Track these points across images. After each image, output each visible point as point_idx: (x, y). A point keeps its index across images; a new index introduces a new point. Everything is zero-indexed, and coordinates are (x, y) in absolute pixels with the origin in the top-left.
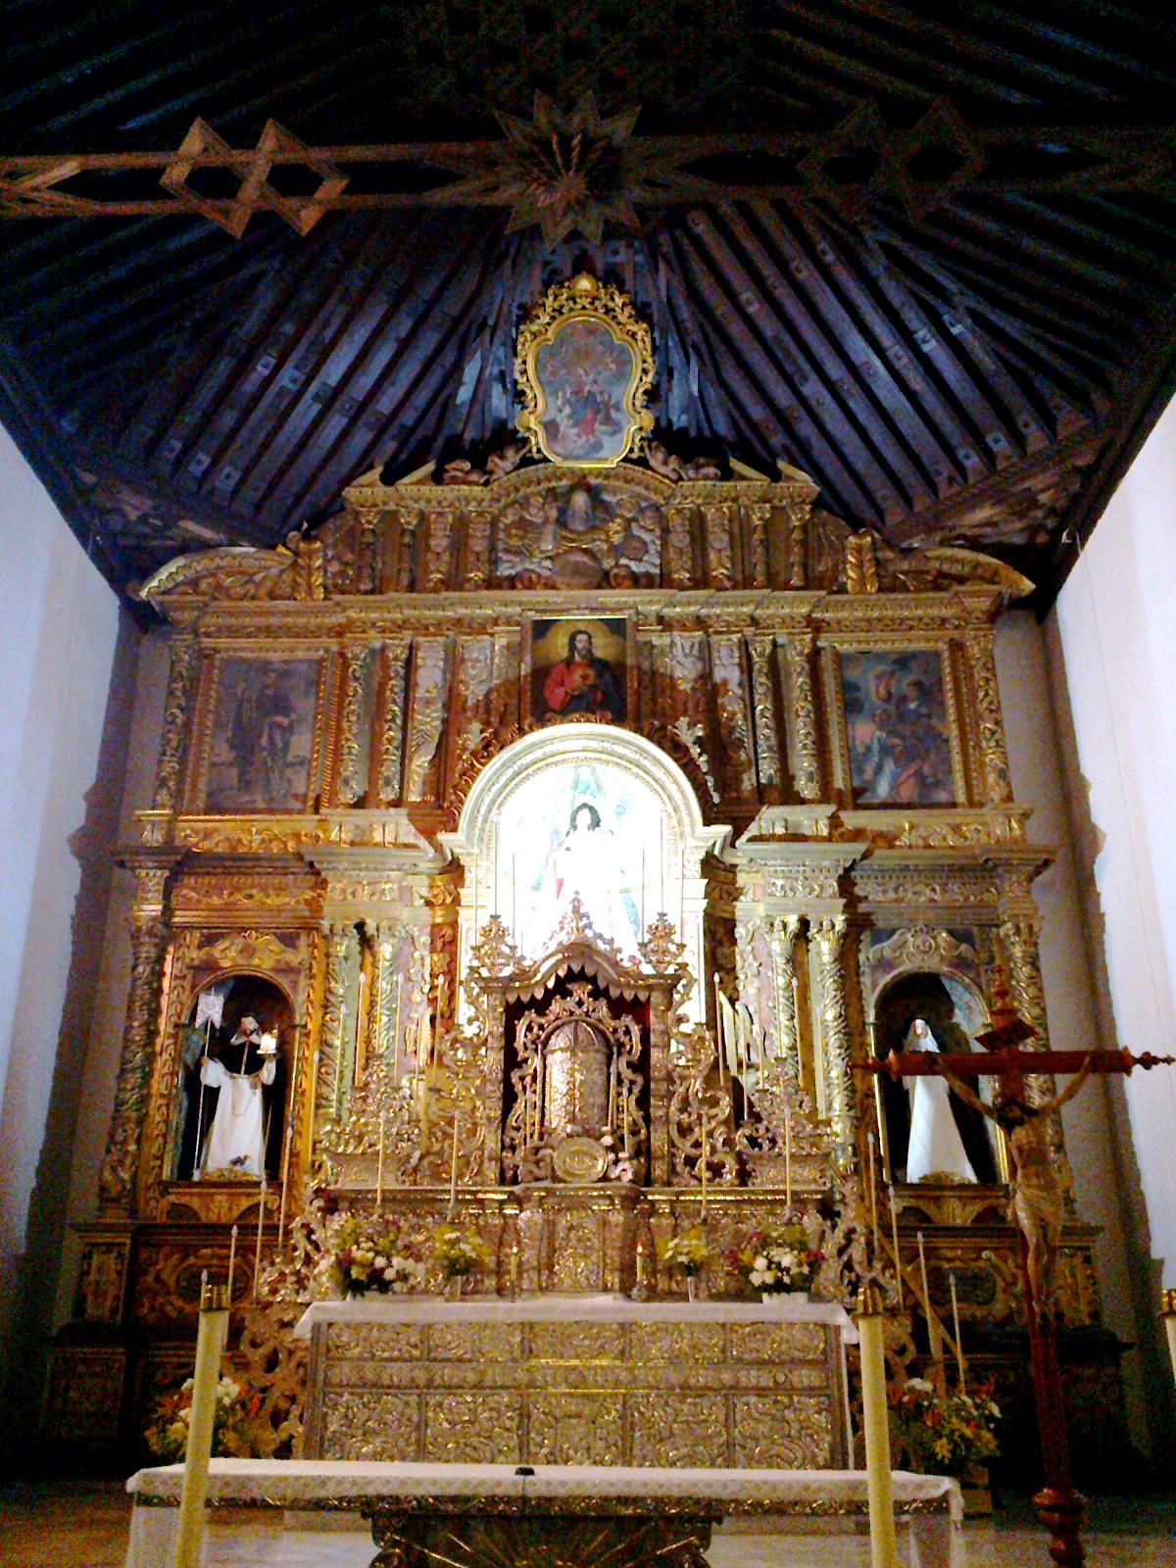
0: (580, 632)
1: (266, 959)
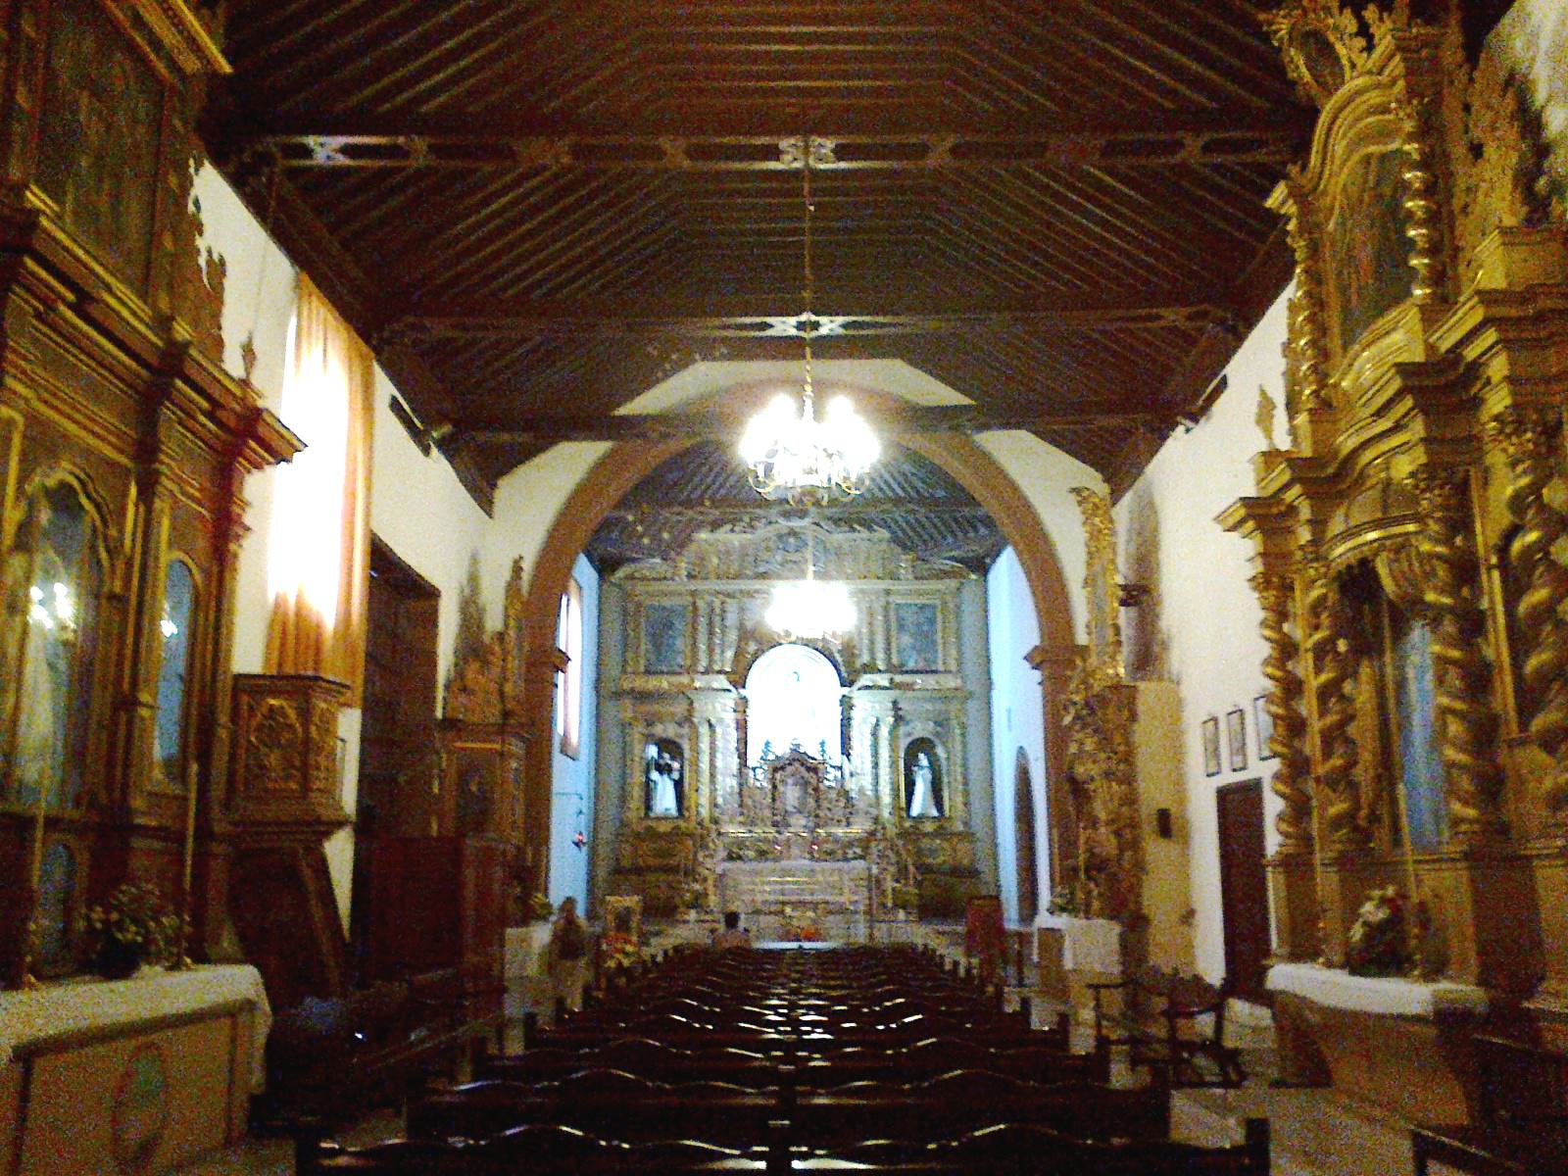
1: (670, 731)
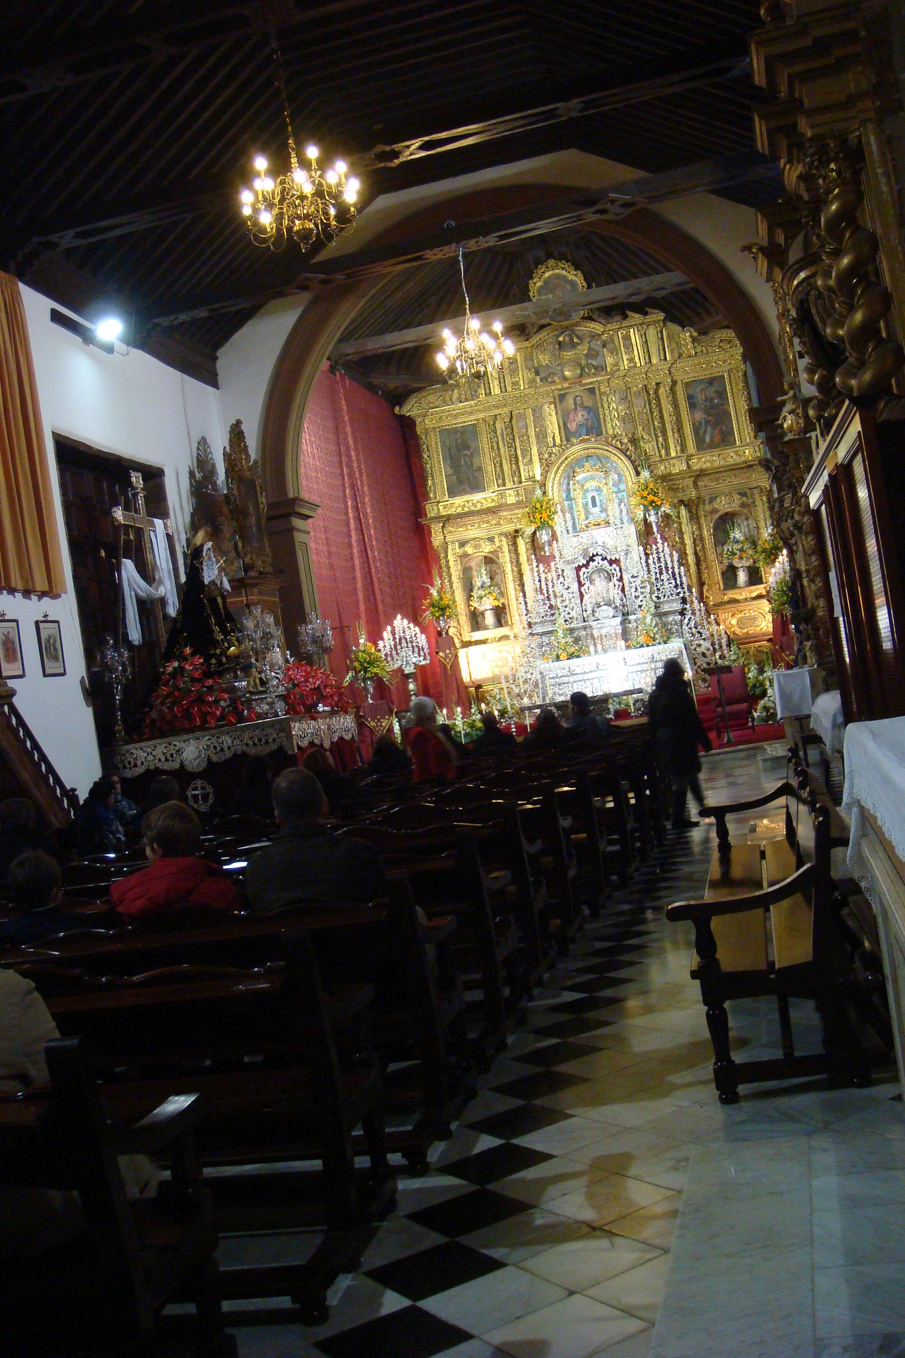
0: (577, 396)
